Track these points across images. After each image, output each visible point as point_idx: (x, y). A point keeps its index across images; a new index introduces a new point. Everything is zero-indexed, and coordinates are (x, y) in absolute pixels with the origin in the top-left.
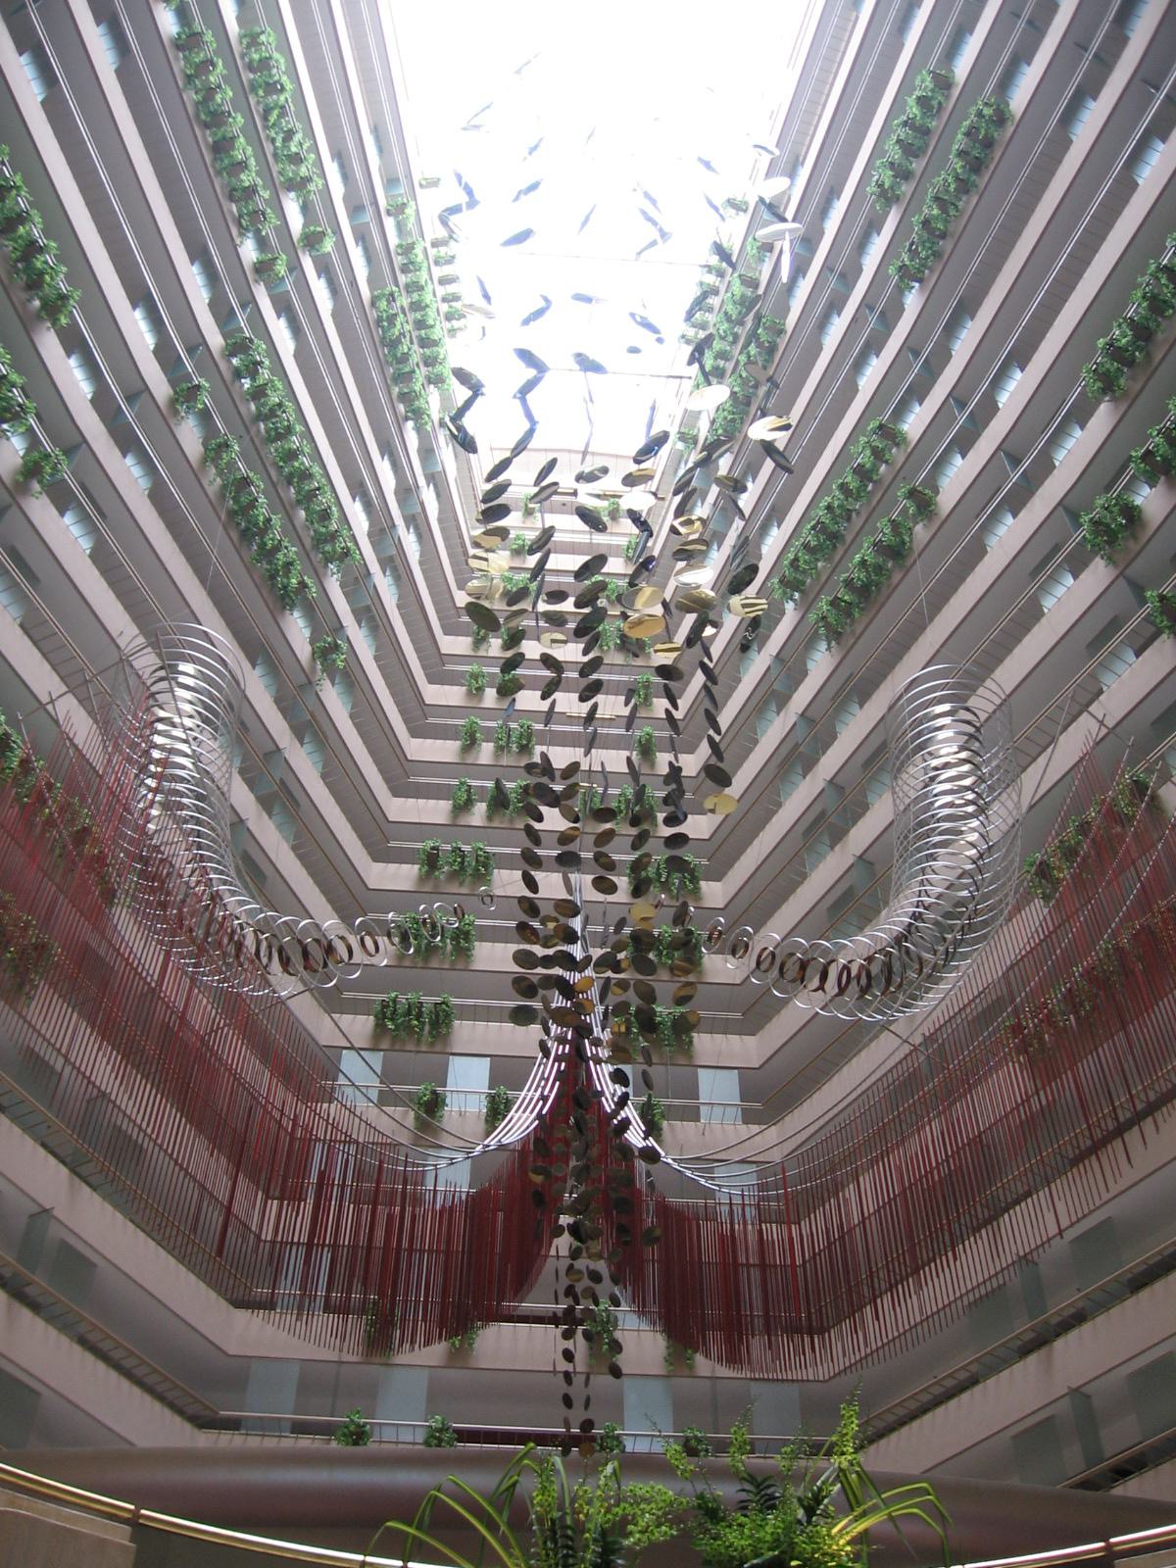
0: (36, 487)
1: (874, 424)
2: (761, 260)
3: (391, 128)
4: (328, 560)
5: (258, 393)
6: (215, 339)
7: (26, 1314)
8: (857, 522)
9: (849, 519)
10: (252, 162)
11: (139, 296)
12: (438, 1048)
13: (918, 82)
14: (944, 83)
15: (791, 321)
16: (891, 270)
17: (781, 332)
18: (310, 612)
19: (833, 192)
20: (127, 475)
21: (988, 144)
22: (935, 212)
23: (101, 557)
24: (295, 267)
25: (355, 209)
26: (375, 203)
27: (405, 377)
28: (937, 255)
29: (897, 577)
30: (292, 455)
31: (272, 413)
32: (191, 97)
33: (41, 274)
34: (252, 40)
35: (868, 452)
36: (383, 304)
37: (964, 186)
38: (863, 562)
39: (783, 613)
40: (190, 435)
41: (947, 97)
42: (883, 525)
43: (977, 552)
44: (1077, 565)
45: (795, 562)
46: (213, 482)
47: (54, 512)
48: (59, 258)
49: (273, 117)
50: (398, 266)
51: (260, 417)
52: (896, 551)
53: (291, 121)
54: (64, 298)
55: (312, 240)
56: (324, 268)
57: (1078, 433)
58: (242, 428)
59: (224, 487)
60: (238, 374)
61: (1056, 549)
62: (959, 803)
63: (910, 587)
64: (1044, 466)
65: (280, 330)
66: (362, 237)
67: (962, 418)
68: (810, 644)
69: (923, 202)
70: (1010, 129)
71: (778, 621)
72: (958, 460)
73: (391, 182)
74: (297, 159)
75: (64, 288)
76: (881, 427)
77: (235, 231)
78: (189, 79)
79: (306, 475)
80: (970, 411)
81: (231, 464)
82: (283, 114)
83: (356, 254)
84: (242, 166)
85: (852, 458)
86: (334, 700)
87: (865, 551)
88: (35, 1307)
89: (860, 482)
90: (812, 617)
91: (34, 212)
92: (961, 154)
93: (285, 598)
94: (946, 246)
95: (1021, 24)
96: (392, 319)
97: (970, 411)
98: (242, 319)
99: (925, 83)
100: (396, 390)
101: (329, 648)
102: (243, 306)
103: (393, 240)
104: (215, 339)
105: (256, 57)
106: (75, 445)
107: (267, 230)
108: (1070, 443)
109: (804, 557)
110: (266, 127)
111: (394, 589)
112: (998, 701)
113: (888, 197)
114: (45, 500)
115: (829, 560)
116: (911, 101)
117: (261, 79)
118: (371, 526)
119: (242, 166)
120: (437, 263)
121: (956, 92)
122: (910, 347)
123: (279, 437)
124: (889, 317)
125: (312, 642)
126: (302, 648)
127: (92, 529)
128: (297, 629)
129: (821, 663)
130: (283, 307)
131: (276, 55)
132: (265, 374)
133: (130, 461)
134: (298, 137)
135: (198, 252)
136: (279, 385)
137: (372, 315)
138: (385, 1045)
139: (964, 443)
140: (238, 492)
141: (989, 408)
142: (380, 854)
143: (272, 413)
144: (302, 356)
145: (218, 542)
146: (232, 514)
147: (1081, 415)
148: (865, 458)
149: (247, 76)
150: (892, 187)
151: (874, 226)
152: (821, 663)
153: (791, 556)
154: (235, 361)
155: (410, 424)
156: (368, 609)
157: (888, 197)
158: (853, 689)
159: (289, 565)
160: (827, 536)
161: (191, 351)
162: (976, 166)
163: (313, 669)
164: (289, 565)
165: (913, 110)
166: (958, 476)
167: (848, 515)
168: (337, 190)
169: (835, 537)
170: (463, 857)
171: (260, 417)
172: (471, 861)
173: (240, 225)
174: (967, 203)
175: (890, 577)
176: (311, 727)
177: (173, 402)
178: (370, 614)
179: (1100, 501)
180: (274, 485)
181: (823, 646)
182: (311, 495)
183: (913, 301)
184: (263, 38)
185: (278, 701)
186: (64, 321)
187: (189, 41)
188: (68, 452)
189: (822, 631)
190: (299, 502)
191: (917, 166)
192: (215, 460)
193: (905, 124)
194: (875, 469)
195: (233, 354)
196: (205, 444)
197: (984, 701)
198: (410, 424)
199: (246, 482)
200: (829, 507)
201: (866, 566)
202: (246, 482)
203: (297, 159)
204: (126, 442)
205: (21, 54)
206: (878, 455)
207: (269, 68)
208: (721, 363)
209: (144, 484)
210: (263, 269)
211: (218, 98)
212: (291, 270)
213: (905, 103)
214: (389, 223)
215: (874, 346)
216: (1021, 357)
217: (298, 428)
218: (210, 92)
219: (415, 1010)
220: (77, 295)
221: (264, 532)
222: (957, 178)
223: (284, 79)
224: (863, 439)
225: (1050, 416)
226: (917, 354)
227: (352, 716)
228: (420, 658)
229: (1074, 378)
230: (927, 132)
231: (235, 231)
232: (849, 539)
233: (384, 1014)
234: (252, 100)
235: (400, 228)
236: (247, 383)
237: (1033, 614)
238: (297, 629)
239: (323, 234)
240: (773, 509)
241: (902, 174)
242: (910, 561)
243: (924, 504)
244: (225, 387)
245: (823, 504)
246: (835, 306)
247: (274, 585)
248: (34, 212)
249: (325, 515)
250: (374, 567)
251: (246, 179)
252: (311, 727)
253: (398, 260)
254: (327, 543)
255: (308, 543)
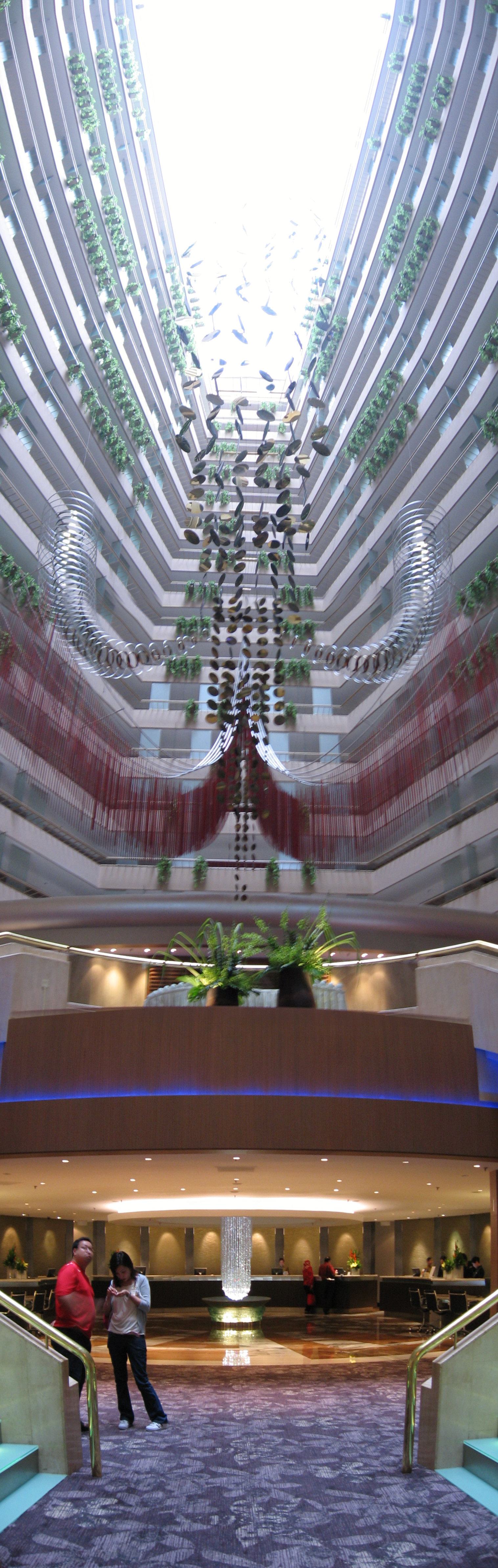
0: (5, 421)
1: (387, 372)
2: (335, 288)
3: (168, 233)
4: (140, 444)
5: (107, 366)
6: (87, 341)
7: (20, 819)
8: (382, 420)
9: (378, 418)
10: (105, 257)
11: (52, 323)
12: (195, 681)
13: (397, 208)
14: (408, 209)
15: (349, 318)
16: (392, 297)
17: (345, 323)
18: (132, 471)
19: (365, 257)
20: (47, 412)
21: (430, 238)
22: (409, 270)
23: (35, 453)
24: (124, 303)
25: (152, 272)
26: (161, 268)
27: (175, 350)
28: (412, 289)
29: (400, 448)
30: (123, 395)
31: (113, 375)
32: (79, 229)
33: (9, 319)
34: (107, 200)
35: (385, 386)
36: (164, 316)
37: (421, 257)
38: (384, 442)
39: (349, 464)
40: (75, 390)
41: (411, 215)
42: (393, 423)
43: (435, 437)
44: (481, 445)
45: (354, 440)
46: (86, 411)
47: (13, 432)
48: (18, 312)
49: (115, 235)
50: (171, 298)
51: (107, 377)
52: (398, 436)
53: (123, 236)
54: (19, 330)
55: (132, 289)
56: (138, 301)
57: (479, 378)
58: (100, 385)
59: (91, 413)
60: (97, 358)
61: (471, 436)
62: (427, 570)
63: (406, 453)
64: (464, 395)
65: (117, 333)
66: (155, 284)
67: (427, 370)
68: (362, 480)
69: (403, 265)
70: (439, 231)
71: (347, 468)
72: (426, 390)
73: (168, 256)
74: (125, 253)
75: (19, 325)
76: (391, 373)
77: (97, 289)
78: (79, 221)
79: (129, 404)
80: (430, 366)
81: (94, 403)
82: (119, 233)
83: (152, 293)
84: (100, 259)
85: (377, 389)
86: (144, 514)
87: (385, 436)
88: (24, 815)
89: (382, 400)
90: (362, 468)
91: (7, 291)
92: (419, 242)
93: (120, 466)
94: (416, 285)
95: (439, 184)
96: (168, 323)
97: (430, 366)
98: (99, 331)
99: (400, 210)
100: (171, 357)
101: (141, 489)
102: (100, 324)
103: (169, 284)
104: (87, 341)
105: (108, 209)
106: (23, 399)
107: (112, 287)
108: (475, 383)
109: (358, 437)
110: (112, 239)
111: (171, 455)
112: (441, 518)
113: (388, 261)
114: (9, 427)
115: (370, 438)
116: (395, 217)
117: (110, 218)
118: (160, 425)
119: (100, 259)
120: (189, 292)
121: (414, 213)
122: (403, 333)
123: (116, 387)
124: (393, 318)
125: (133, 485)
126: (128, 489)
127: (31, 441)
128: (126, 481)
129: (367, 491)
130: (119, 322)
131: (117, 207)
132: (110, 357)
133: (48, 404)
134: (126, 243)
135: (80, 300)
136: (116, 362)
137: (160, 321)
138: (171, 680)
139: (429, 381)
140: (97, 415)
141: (439, 365)
142: (167, 587)
143: (113, 375)
144: (127, 345)
145: (89, 441)
146: (95, 426)
147: (480, 369)
148: (384, 388)
149: (104, 217)
150: (390, 257)
151: (383, 274)
152: (367, 491)
153: (352, 436)
154: (96, 351)
155: (178, 372)
156: (159, 467)
157: (388, 261)
158: (381, 503)
159: (121, 449)
160: (368, 428)
161: (75, 348)
162: (426, 248)
163: (134, 499)
164: (121, 449)
165: (396, 222)
166: (426, 398)
167: (378, 416)
168: (144, 263)
169: (372, 427)
170: (205, 588)
171: (107, 377)
172: (208, 590)
173: (99, 286)
174: (424, 265)
175: (397, 448)
176: (134, 527)
177: (68, 374)
178: (160, 469)
179: (489, 414)
180: (115, 410)
181: (368, 481)
182: (131, 414)
183: (403, 311)
184: (112, 200)
185: (118, 516)
186: (18, 341)
187: (79, 204)
188: (19, 403)
189: (367, 475)
190: (126, 417)
191: (400, 246)
192: (87, 401)
193: (394, 228)
194: (388, 394)
195: (95, 348)
196: (82, 393)
197: (436, 517)
198: (178, 372)
199: (101, 411)
200: (369, 413)
201: (386, 443)
202: (101, 411)
203: (125, 253)
204: (46, 395)
205: (5, 216)
206: (390, 387)
207: (114, 212)
208: (319, 337)
209: (55, 415)
210: (109, 305)
211: (91, 229)
212: (122, 304)
213: (393, 219)
214: (168, 276)
215: (387, 332)
216: (452, 339)
217: (125, 382)
218: (87, 227)
219: (184, 663)
220: (25, 328)
221: (108, 435)
222: (418, 254)
223: (121, 217)
224: (383, 380)
225: (466, 370)
226: (406, 337)
227: (153, 521)
228: (469, 127)
229: (476, 353)
230: (403, 231)
231: (97, 289)
232: (378, 428)
233: (171, 665)
234: (106, 227)
235: (173, 277)
236: (101, 361)
237: (461, 469)
238: (126, 481)
239: (137, 286)
240: (344, 411)
241: (393, 250)
242: (405, 441)
243: (411, 412)
244: (91, 365)
245: (366, 411)
246: (369, 311)
247: (115, 459)
248: (7, 291)
249: (138, 423)
250: (161, 445)
251: (102, 265)
252: (134, 527)
253: (172, 294)
254: (139, 437)
255: (130, 437)
